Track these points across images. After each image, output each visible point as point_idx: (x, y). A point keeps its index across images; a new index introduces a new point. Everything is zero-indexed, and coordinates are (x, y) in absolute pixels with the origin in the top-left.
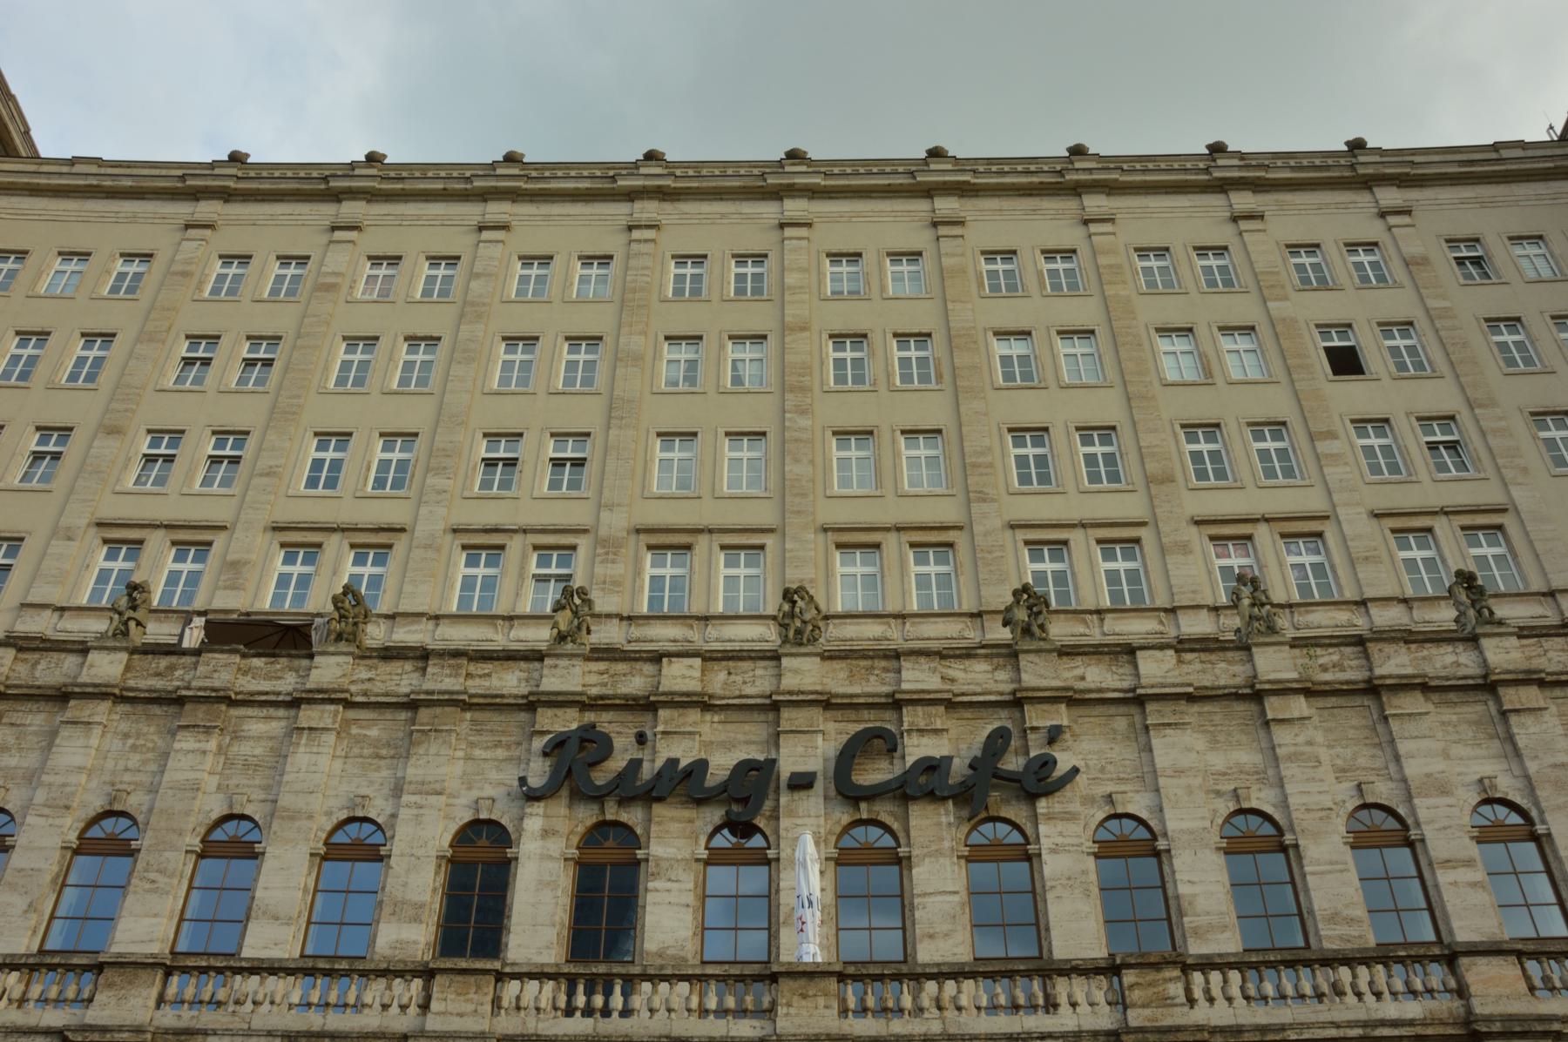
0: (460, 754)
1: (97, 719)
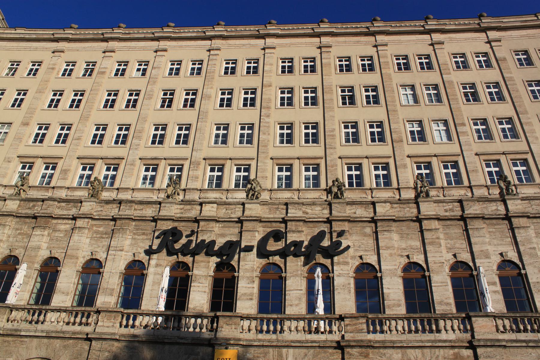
0: (131, 237)
1: (7, 224)
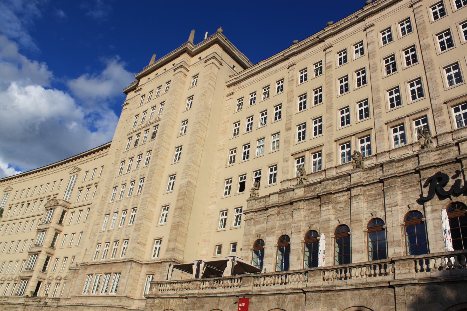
0: (401, 192)
